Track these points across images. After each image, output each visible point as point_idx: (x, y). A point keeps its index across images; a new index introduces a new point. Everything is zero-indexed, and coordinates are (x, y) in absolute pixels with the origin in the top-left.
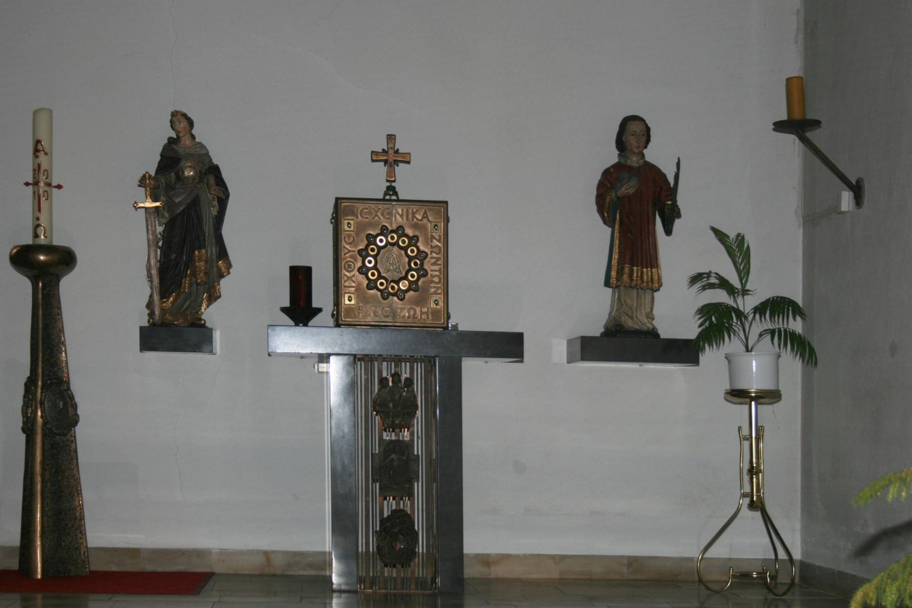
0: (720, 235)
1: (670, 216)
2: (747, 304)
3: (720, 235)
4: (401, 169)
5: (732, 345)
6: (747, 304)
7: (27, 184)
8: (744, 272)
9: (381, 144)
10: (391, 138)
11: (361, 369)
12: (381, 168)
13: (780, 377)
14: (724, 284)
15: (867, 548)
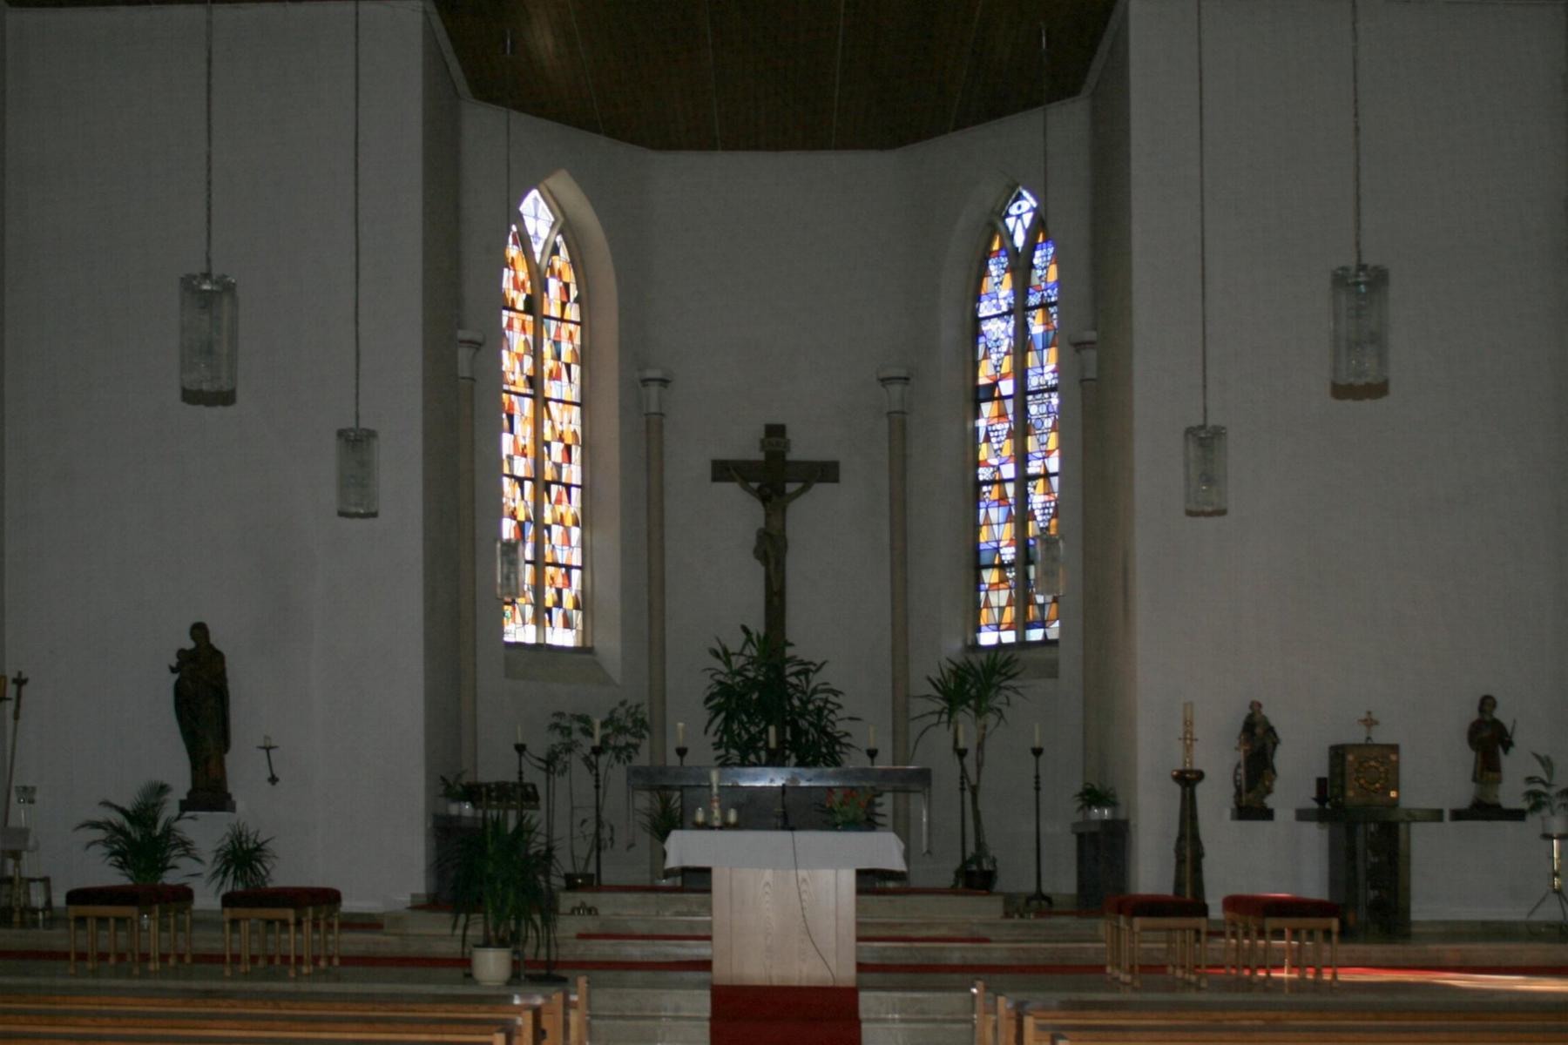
0: (1537, 756)
1: (1507, 744)
2: (1553, 791)
3: (1537, 756)
4: (1374, 728)
5: (1546, 812)
6: (1553, 791)
7: (1180, 739)
8: (1550, 773)
9: (1363, 716)
10: (1369, 713)
11: (1051, 1018)
12: (1364, 728)
13: (959, 828)
14: (1542, 782)
15: (553, 547)
